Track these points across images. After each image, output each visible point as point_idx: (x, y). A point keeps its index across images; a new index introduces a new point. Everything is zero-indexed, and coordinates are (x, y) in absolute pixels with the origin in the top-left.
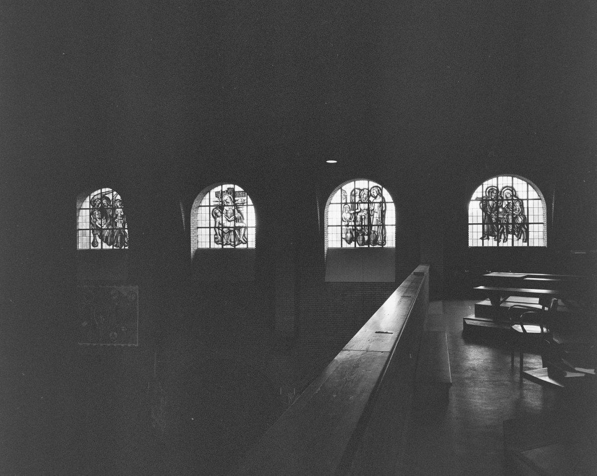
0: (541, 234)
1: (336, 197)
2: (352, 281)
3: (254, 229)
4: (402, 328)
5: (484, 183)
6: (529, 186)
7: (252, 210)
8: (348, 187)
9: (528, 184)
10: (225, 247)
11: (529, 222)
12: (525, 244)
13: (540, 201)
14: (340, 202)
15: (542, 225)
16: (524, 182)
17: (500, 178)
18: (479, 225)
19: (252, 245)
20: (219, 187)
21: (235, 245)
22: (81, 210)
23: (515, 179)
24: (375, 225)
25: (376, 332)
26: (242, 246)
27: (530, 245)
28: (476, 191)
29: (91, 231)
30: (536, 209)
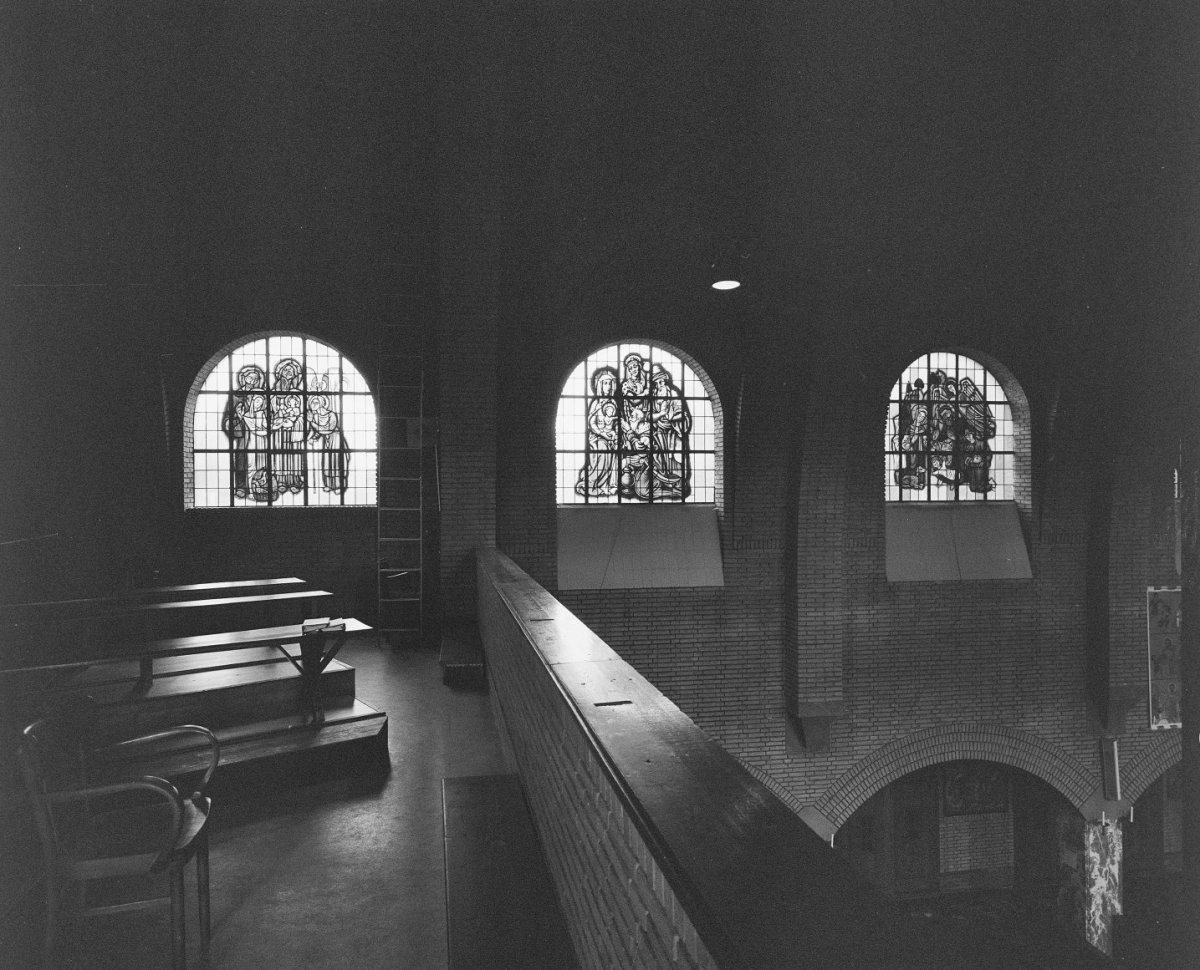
0: (199, 481)
1: (576, 382)
2: (670, 585)
3: (374, 456)
4: (565, 690)
5: (590, 358)
6: (686, 366)
7: (368, 405)
8: (606, 356)
9: (683, 363)
10: (592, 500)
11: (228, 455)
12: (334, 500)
13: (708, 403)
14: (228, 389)
15: (1012, 456)
16: (978, 366)
17: (274, 341)
18: (708, 455)
19: (362, 490)
20: (921, 359)
21: (270, 495)
22: (201, 396)
23: (310, 343)
24: (889, 453)
25: (629, 702)
26: (288, 500)
27: (346, 502)
28: (357, 371)
29: (904, 457)
30: (360, 420)
